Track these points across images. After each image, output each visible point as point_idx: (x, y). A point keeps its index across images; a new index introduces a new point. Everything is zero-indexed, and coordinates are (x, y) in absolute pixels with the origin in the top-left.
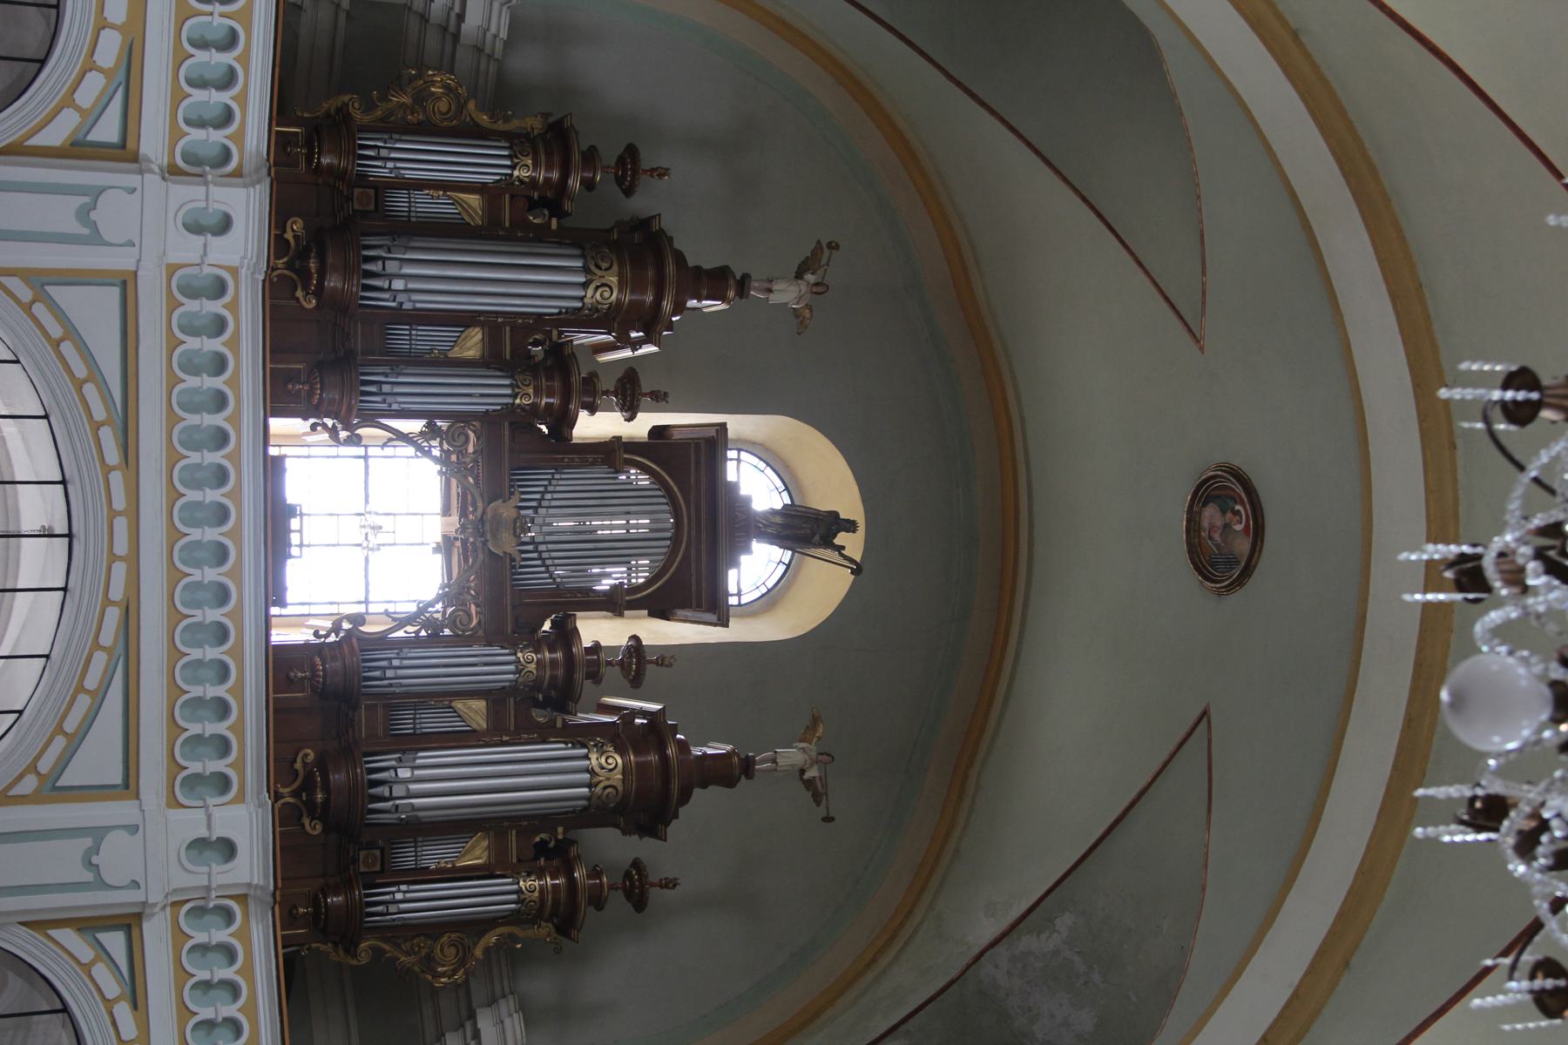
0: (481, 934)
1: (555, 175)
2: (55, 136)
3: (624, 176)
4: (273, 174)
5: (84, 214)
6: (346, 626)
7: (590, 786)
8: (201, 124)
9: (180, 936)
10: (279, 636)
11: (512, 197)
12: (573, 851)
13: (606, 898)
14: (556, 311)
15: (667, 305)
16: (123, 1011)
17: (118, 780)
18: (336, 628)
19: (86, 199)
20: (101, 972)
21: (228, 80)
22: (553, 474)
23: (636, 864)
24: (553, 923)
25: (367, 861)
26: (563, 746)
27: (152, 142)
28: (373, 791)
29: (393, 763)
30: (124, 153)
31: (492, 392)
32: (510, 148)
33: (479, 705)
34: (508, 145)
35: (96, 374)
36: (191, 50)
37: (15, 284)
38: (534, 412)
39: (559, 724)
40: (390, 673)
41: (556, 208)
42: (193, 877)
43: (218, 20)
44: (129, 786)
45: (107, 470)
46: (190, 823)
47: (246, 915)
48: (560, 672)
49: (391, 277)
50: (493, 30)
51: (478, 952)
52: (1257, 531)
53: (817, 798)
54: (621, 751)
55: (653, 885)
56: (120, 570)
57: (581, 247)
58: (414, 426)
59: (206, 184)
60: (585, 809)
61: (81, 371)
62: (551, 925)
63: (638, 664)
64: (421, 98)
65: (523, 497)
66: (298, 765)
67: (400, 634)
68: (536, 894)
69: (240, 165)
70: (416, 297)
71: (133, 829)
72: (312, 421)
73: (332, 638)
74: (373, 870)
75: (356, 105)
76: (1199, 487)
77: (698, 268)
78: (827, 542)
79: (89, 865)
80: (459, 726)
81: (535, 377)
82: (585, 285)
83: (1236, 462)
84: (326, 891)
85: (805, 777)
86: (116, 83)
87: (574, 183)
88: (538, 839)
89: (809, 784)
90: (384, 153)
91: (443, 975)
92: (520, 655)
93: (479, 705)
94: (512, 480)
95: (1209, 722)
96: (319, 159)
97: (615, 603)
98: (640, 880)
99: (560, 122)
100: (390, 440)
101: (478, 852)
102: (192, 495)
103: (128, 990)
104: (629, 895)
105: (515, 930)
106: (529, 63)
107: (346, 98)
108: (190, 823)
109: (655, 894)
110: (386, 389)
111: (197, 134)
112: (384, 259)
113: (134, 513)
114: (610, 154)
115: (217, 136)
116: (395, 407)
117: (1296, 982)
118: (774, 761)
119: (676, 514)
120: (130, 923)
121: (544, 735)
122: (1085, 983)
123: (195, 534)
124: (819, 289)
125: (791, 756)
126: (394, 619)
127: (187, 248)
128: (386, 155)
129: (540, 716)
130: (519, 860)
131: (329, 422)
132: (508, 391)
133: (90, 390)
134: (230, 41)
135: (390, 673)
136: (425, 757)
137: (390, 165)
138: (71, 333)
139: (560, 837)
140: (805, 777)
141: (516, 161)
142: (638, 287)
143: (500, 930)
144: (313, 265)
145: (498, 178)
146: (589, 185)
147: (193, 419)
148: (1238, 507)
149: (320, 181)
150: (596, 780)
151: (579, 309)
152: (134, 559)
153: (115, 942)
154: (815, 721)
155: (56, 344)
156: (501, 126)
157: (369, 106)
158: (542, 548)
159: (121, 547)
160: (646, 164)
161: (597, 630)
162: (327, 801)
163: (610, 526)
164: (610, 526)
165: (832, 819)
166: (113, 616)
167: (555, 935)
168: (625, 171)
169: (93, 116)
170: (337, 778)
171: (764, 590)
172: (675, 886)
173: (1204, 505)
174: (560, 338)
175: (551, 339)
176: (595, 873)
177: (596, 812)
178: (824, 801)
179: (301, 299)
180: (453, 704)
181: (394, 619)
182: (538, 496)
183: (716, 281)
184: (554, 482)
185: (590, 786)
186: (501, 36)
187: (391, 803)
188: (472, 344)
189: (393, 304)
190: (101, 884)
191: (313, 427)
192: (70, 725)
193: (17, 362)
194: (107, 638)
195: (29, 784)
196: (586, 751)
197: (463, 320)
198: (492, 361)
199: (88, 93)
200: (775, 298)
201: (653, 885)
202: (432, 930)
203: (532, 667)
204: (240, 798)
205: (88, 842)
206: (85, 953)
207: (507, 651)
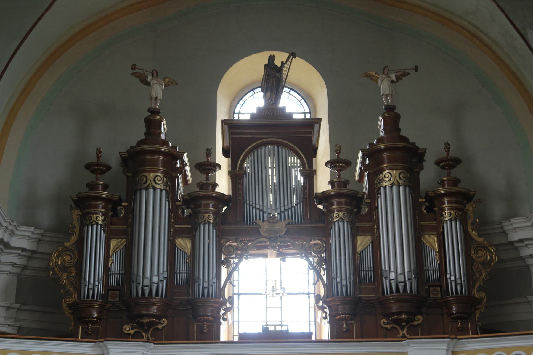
0: (471, 238)
1: (101, 204)
3: (101, 170)
6: (321, 304)
7: (399, 186)
10: (326, 335)
11: (112, 224)
12: (431, 194)
14: (167, 203)
15: (164, 149)
18: (322, 308)
24: (467, 203)
25: (435, 294)
26: (379, 199)
29: (388, 281)
33: (359, 239)
34: (86, 227)
38: (217, 214)
39: (369, 201)
40: (344, 283)
48: (343, 200)
50: (30, 234)
51: (480, 240)
53: (406, 74)
54: (382, 171)
55: (448, 155)
57: (137, 190)
60: (410, 188)
63: (339, 162)
64: (64, 269)
65: (258, 218)
66: (389, 327)
67: (325, 278)
68: (452, 212)
72: (222, 320)
73: (327, 310)
77: (146, 134)
78: (279, 70)
80: (370, 249)
82: (155, 189)
84: (450, 314)
88: (425, 211)
89: (399, 78)
90: (91, 286)
91: (491, 257)
93: (359, 239)
94: (250, 224)
96: (94, 318)
98: (445, 161)
100: (231, 283)
104: (453, 167)
105: (469, 222)
107: (64, 305)
110: (206, 285)
112: (143, 286)
114: (90, 177)
116: (214, 280)
118: (387, 96)
119: (266, 144)
124: (155, 74)
125: (385, 87)
126: (318, 280)
129: (365, 210)
131: (222, 312)
136: (385, 266)
137: (97, 283)
139: (424, 200)
141: (94, 222)
142: (155, 163)
143: (470, 229)
144: (146, 320)
145: (102, 231)
146: (105, 187)
151: (166, 191)
154: (367, 75)
156: (77, 230)
157: (68, 294)
160: (94, 159)
162: (407, 313)
163: (272, 176)
164: (272, 176)
167: (472, 203)
168: (99, 170)
174: (180, 201)
175: (181, 205)
176: (442, 183)
179: (163, 326)
181: (318, 280)
182: (258, 211)
185: (399, 186)
187: (407, 282)
191: (225, 320)
197: (172, 248)
200: (160, 96)
201: (448, 155)
202: (469, 262)
207: (333, 226)
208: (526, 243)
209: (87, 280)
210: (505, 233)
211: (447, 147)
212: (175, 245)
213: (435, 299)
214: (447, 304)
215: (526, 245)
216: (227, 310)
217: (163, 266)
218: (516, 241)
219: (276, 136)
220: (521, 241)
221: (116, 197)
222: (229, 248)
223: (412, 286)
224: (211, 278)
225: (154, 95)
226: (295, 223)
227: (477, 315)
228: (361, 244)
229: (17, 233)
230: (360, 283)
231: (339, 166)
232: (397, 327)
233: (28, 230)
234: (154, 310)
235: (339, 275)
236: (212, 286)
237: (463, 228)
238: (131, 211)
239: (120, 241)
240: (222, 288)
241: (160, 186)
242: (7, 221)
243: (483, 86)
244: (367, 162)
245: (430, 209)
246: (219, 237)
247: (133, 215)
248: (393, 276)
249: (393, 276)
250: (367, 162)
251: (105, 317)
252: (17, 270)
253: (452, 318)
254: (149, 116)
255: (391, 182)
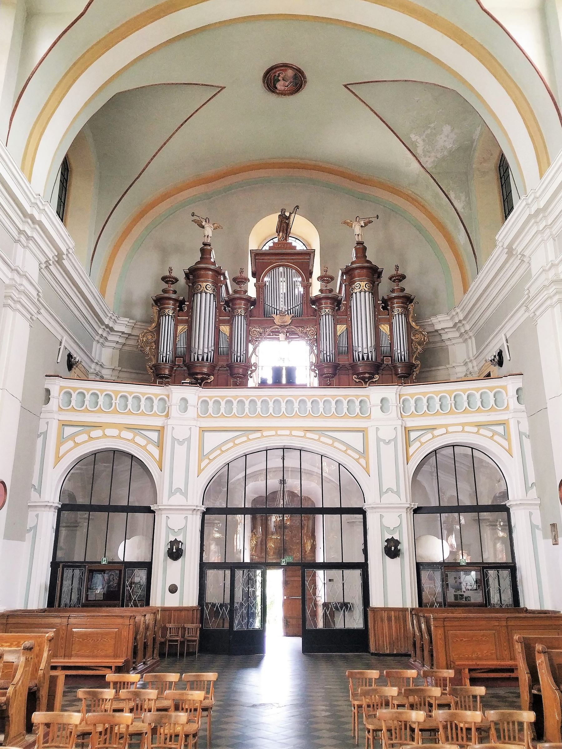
0: (412, 327)
1: (171, 302)
2: (155, 452)
3: (172, 281)
4: (168, 385)
5: (181, 443)
6: (313, 367)
7: (365, 292)
8: (152, 407)
9: (412, 415)
10: (316, 384)
11: (178, 316)
12: (386, 298)
13: (401, 287)
14: (214, 302)
15: (212, 267)
16: (436, 432)
17: (361, 434)
18: (314, 371)
19: (176, 442)
20: (423, 439)
21: (137, 398)
22: (266, 305)
23: (390, 279)
24: (409, 304)
25: (387, 361)
26: (352, 301)
27: (158, 422)
28: (365, 358)
29: (357, 353)
30: (161, 431)
31: (240, 322)
32: (163, 316)
33: (338, 327)
34: (162, 317)
35: (233, 440)
36: (128, 409)
37: (203, 465)
38: (246, 310)
39: (345, 302)
40: (328, 354)
41: (182, 302)
42: (393, 411)
43: (118, 401)
44: (363, 431)
45: (263, 436)
46: (376, 412)
47: (406, 395)
48: (329, 301)
49: (203, 352)
50: (126, 323)
51: (417, 328)
52: (286, 66)
53: (370, 222)
54: (354, 283)
55: (397, 273)
56: (294, 433)
57: (195, 294)
58: (251, 347)
59: (171, 405)
60: (372, 294)
61: (231, 444)
62: (409, 305)
63: (326, 277)
64: (147, 343)
65: (273, 313)
66: (357, 380)
67: (316, 351)
68: (399, 309)
69: (166, 395)
70: (210, 345)
71: (377, 429)
72: (249, 377)
73: (317, 372)
74: (390, 359)
75: (150, 364)
76: (270, 90)
77: (201, 258)
78: (288, 218)
79: (389, 442)
80: (345, 334)
81: (236, 309)
82: (206, 293)
83: (262, 74)
84: (396, 374)
85: (364, 225)
86: (138, 433)
87: (174, 296)
88: (382, 309)
89: (366, 224)
90: (165, 355)
91: (424, 339)
92: (323, 314)
93: (338, 327)
94: (268, 317)
95: (349, 84)
96: (166, 375)
97: (307, 286)
98: (396, 277)
99: (154, 301)
100: (255, 354)
101: (385, 328)
102: (271, 410)
103: (430, 431)
104: (400, 281)
105: (410, 316)
106: (139, 312)
107: (148, 367)
108: (376, 412)
109: (400, 272)
110: (239, 354)
111: (155, 408)
112: (198, 355)
113: (276, 428)
114: (165, 286)
115: (156, 402)
116: (245, 352)
117: (441, 34)
118: (358, 235)
119: (280, 266)
120: (407, 431)
121: (349, 307)
122: (435, 129)
123: (283, 409)
124: (207, 220)
125: (357, 229)
126: (311, 353)
127: (192, 412)
128: (165, 354)
129: (343, 308)
130: (388, 315)
131: (249, 372)
132: (240, 317)
133: (237, 442)
134: (125, 397)
135: (328, 354)
136: (355, 344)
137: (168, 353)
138: (219, 447)
139: (381, 302)
140: (364, 225)
141: (167, 314)
142: (206, 276)
143: (410, 321)
144: (199, 376)
145: (172, 320)
146: (175, 292)
147: (247, 410)
148: (277, 74)
149: (174, 375)
150: (363, 290)
151: (214, 295)
152: (291, 429)
153: (413, 435)
154: (345, 223)
155: (223, 452)
156: (156, 319)
157: (150, 360)
158: (289, 308)
159: (287, 432)
160: (167, 274)
161: (316, 289)
162: (369, 373)
163: (283, 288)
164: (283, 288)
165: (377, 215)
166: (309, 435)
167: (412, 304)
168: (170, 281)
169: (149, 440)
170: (361, 370)
171: (310, 292)
172: (398, 266)
173: (276, 88)
174: (223, 302)
175: (224, 305)
176: (393, 291)
177: (374, 291)
178: (370, 219)
179: (211, 380)
180: (338, 335)
181: (311, 353)
182: (273, 309)
183: (205, 251)
184: (269, 304)
185: (365, 292)
186: (71, 246)
187: (369, 353)
188: (225, 329)
189: (212, 352)
190: (396, 438)
191: (251, 377)
192: (344, 448)
193: (228, 464)
194: (316, 437)
195: (363, 461)
196: (354, 293)
197: (217, 332)
198: (230, 323)
199: (142, 442)
200: (210, 235)
201: (397, 273)
202: (410, 342)
203: (327, 310)
204: (368, 396)
205: (381, 443)
206: (417, 444)
207: (322, 318)
208: (446, 330)
209: (162, 351)
210: (433, 325)
211: (397, 268)
212: (220, 330)
213: (387, 365)
214: (395, 367)
215: (446, 332)
216: (253, 371)
217: (212, 342)
218: (439, 330)
219: (285, 261)
220: (443, 329)
221: (181, 298)
222: (254, 332)
223: (372, 355)
224: (242, 350)
225: (207, 234)
226: (297, 317)
227: (415, 375)
228: (340, 330)
229: (118, 321)
230: (339, 353)
231: (327, 280)
232: (363, 382)
233: (125, 320)
234: (205, 370)
235: (325, 349)
236: (243, 355)
237: (407, 320)
238: (191, 308)
239: (184, 327)
240: (250, 357)
241: (210, 291)
242: (111, 313)
243: (420, 233)
244: (345, 278)
245: (385, 308)
246: (248, 325)
247: (192, 311)
248: (360, 349)
249: (360, 349)
250: (345, 278)
251: (174, 375)
252: (119, 346)
253: (398, 377)
254: (203, 247)
255: (360, 290)
